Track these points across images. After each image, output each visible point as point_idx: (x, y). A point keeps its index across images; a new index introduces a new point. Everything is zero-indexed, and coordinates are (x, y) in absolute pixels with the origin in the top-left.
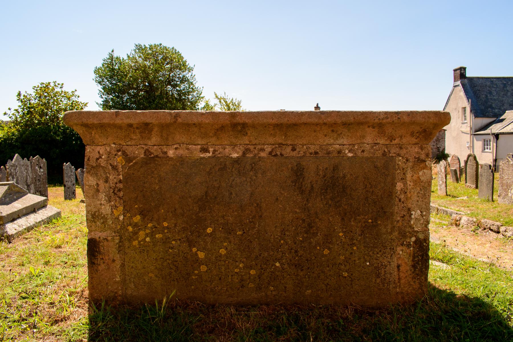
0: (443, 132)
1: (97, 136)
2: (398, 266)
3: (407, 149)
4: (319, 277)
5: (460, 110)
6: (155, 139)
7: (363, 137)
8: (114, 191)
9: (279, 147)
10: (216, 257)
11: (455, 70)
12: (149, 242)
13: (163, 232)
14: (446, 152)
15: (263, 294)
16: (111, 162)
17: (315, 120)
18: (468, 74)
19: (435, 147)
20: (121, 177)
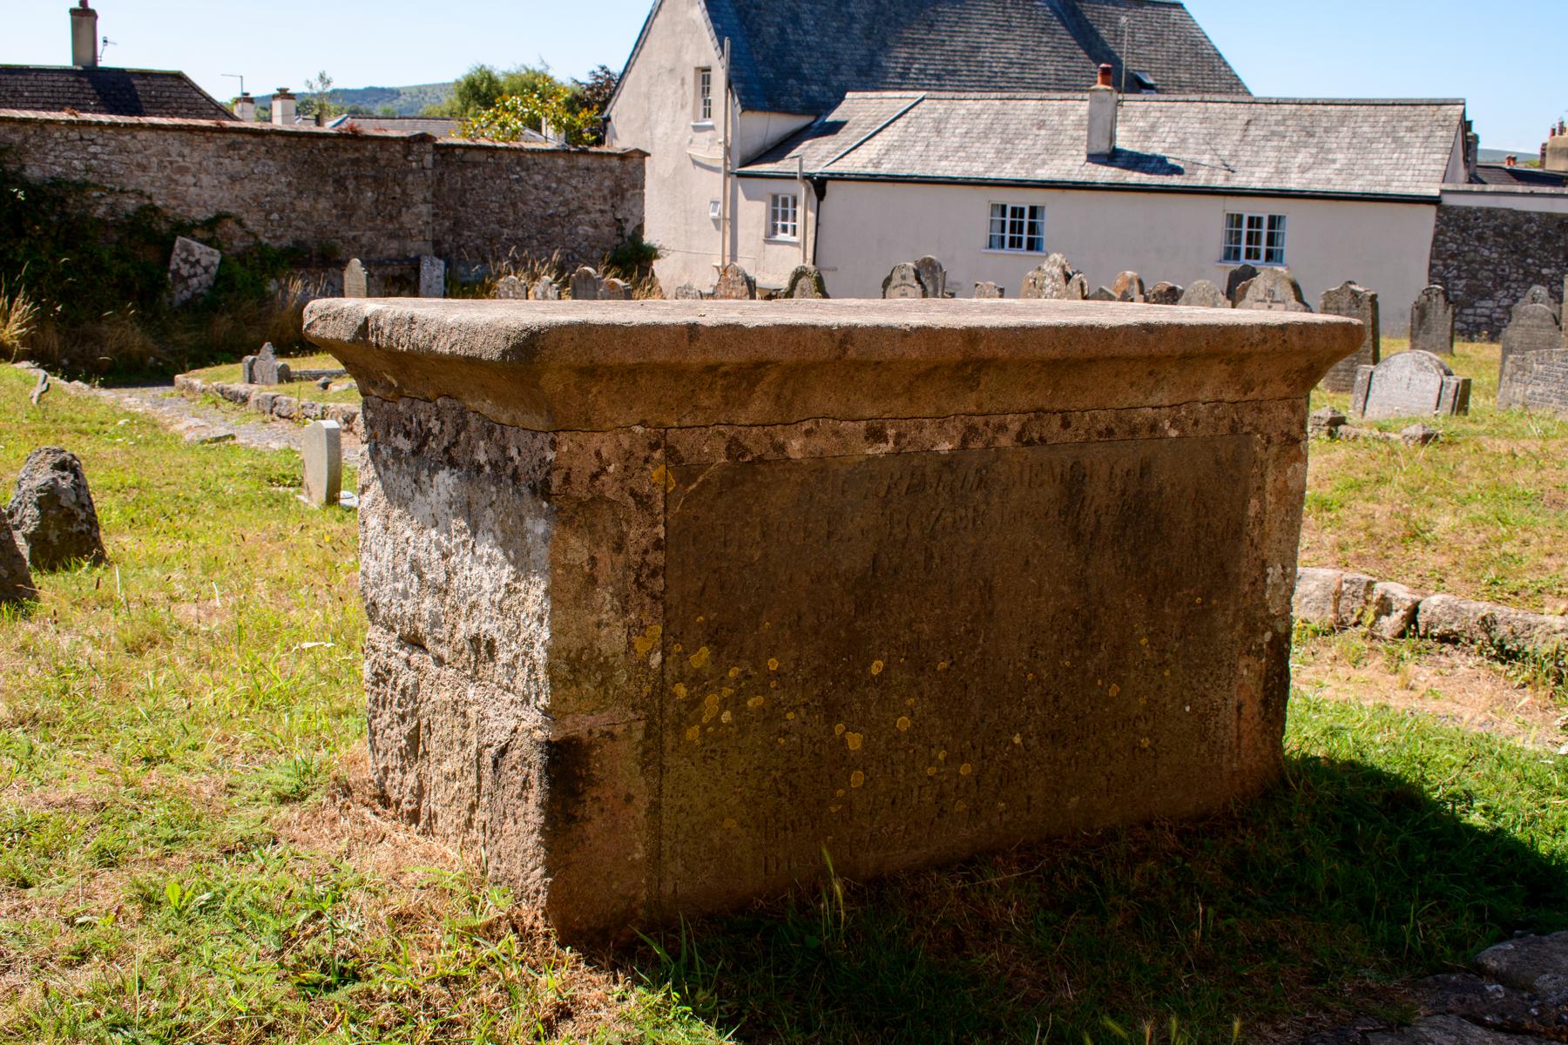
0: (636, 161)
1: (602, 402)
2: (1239, 708)
3: (1269, 411)
4: (1096, 757)
5: (690, 77)
6: (759, 406)
7: (1199, 386)
8: (638, 576)
9: (1038, 418)
10: (888, 742)
12: (730, 725)
13: (764, 690)
14: (649, 238)
15: (984, 824)
16: (633, 483)
17: (1134, 349)
19: (609, 217)
20: (660, 531)
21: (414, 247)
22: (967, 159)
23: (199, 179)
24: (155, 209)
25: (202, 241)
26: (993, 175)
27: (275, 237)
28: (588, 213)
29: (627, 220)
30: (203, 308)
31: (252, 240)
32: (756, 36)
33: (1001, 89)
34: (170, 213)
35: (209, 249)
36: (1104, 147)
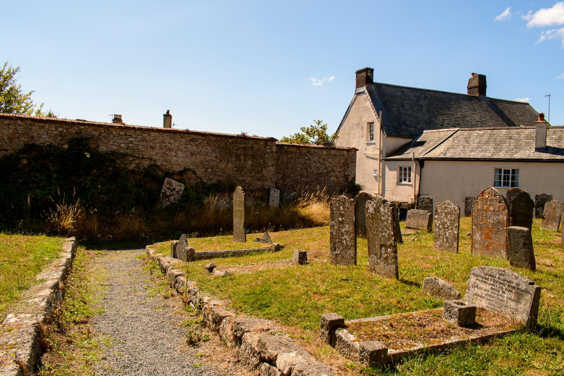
5: (365, 126)
11: (358, 72)
18: (377, 79)
21: (267, 184)
22: (482, 151)
23: (177, 154)
24: (157, 166)
25: (177, 180)
26: (496, 157)
27: (209, 179)
28: (335, 172)
29: (349, 175)
30: (173, 209)
31: (199, 180)
32: (390, 111)
33: (489, 126)
34: (164, 168)
35: (179, 184)
36: (542, 145)
